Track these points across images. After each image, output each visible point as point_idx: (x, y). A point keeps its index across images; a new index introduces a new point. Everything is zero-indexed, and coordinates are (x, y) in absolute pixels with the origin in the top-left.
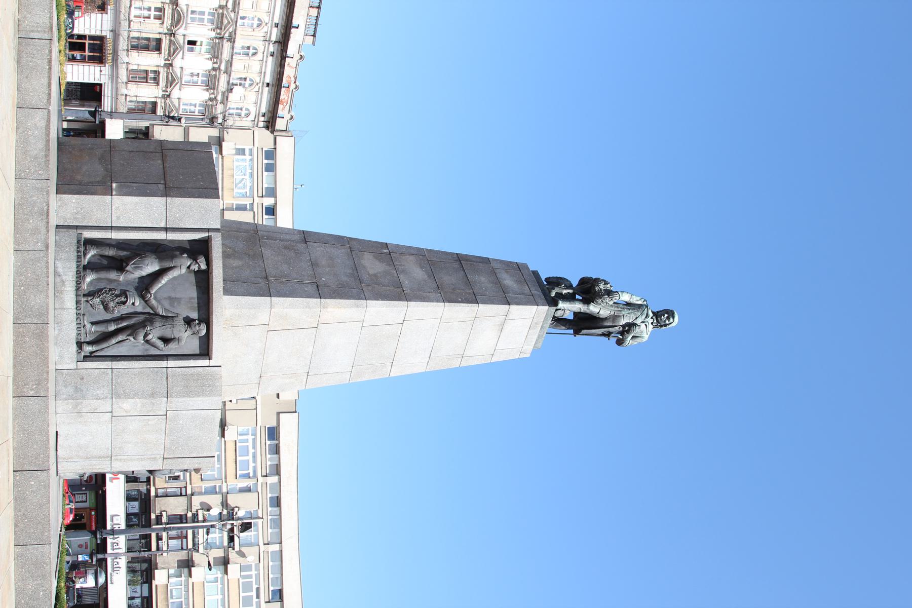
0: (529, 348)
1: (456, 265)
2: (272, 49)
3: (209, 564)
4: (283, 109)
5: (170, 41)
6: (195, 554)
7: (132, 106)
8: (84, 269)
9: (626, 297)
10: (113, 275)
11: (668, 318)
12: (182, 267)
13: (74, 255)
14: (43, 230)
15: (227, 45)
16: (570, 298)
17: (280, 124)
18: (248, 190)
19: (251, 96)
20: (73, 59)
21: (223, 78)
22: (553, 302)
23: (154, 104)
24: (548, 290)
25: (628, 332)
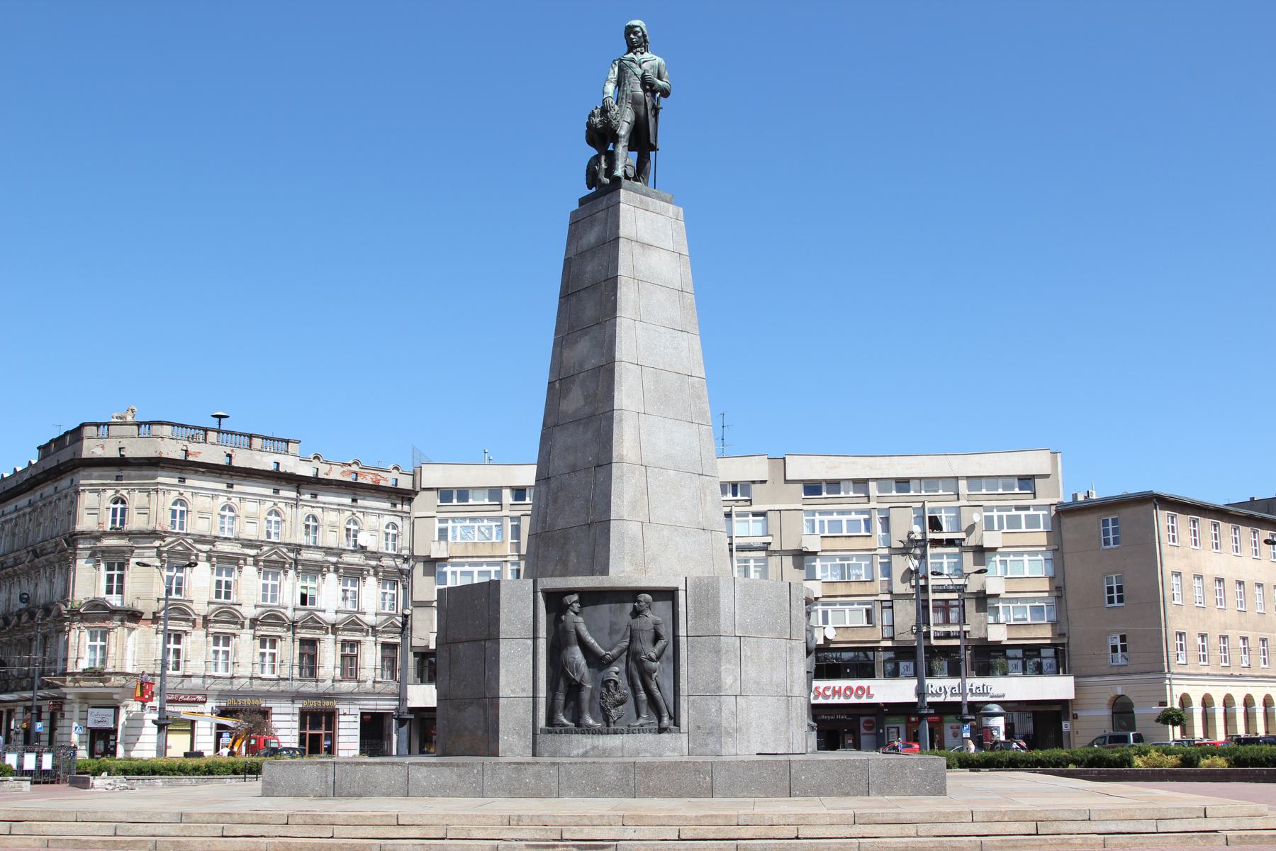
0: (672, 209)
1: (573, 300)
2: (307, 497)
3: (979, 572)
4: (385, 479)
5: (302, 627)
6: (969, 590)
7: (387, 674)
8: (580, 727)
9: (610, 88)
10: (586, 695)
11: (635, 33)
12: (577, 621)
13: (564, 737)
14: (537, 768)
15: (305, 555)
16: (611, 159)
17: (405, 483)
18: (494, 524)
19: (371, 521)
20: (330, 750)
21: (347, 558)
22: (616, 183)
23: (385, 646)
24: (602, 190)
25: (652, 85)
